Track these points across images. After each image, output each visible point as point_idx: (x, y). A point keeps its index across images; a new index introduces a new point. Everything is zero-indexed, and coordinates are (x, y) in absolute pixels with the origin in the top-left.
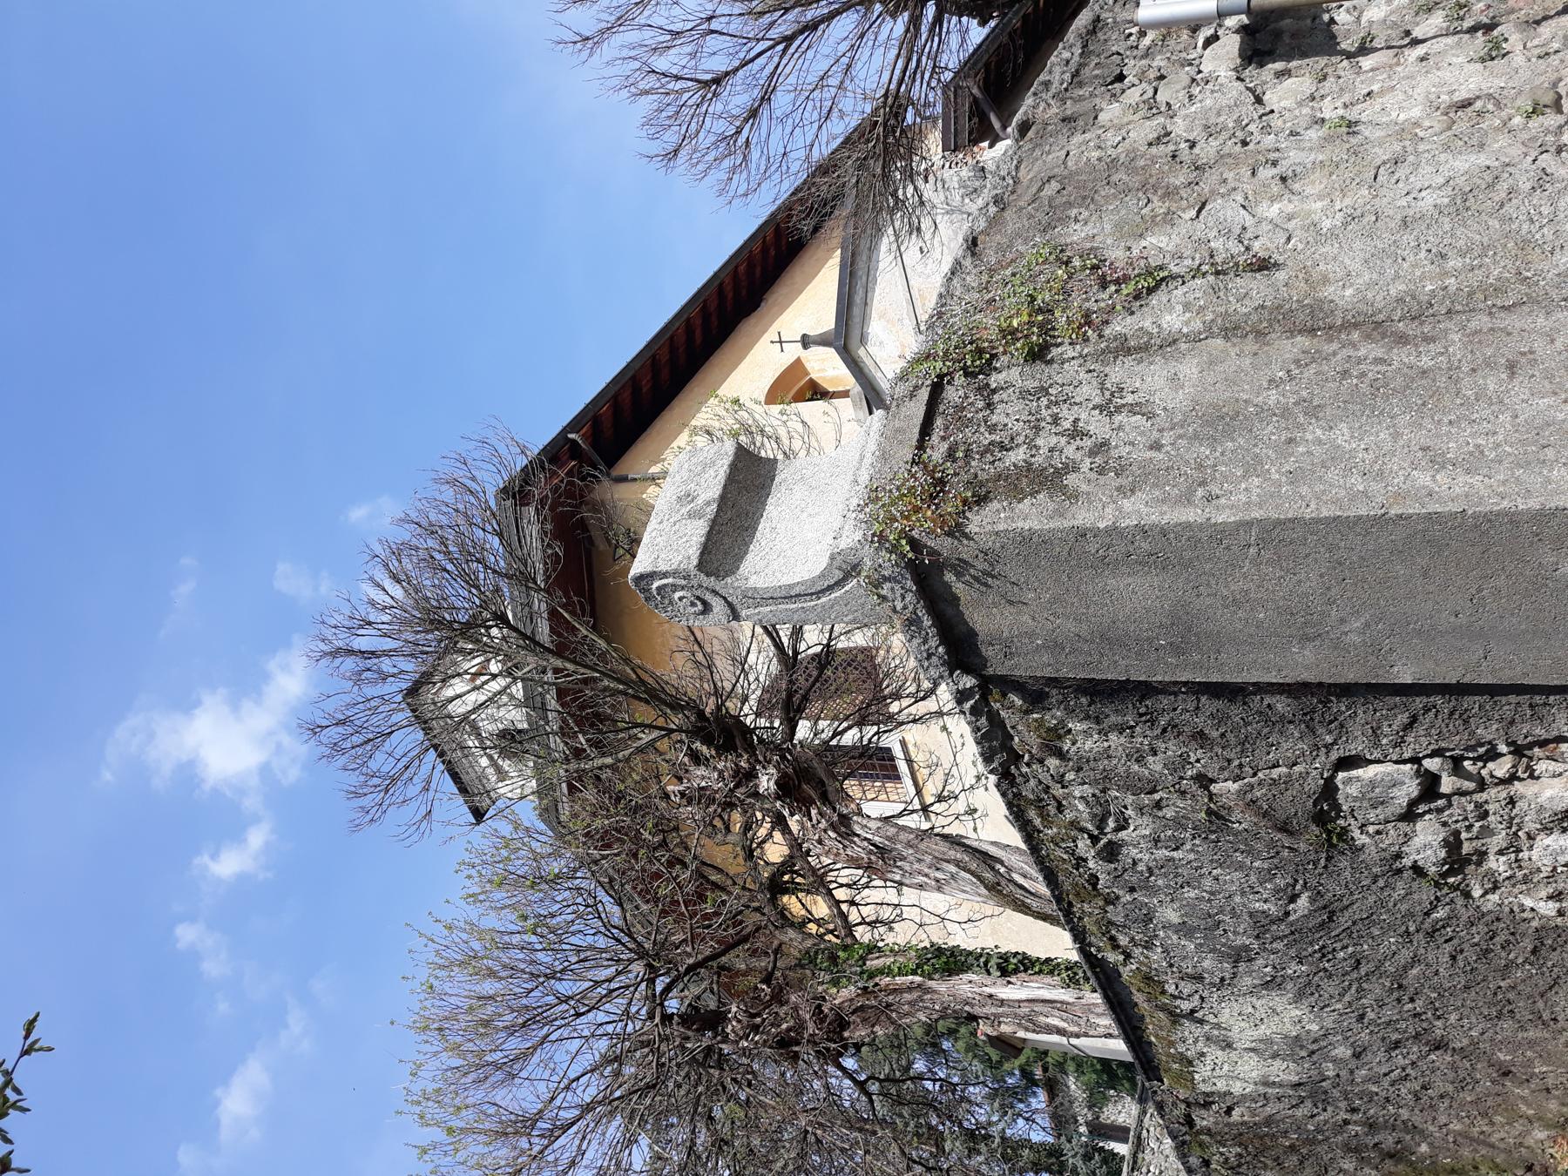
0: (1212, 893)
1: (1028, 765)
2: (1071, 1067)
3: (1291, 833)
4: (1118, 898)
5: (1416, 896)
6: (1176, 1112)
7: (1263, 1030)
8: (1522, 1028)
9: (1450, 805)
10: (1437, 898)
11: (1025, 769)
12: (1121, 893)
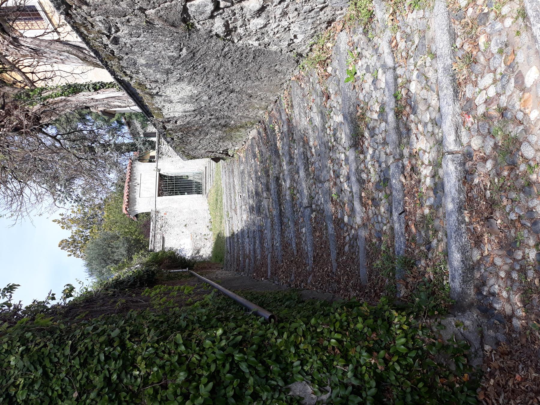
0: (154, 52)
1: (75, 9)
2: (133, 117)
3: (175, 27)
4: (123, 58)
5: (218, 44)
6: (160, 126)
7: (181, 95)
8: (254, 82)
9: (224, 12)
10: (225, 44)
11: (74, 12)
12: (123, 56)
